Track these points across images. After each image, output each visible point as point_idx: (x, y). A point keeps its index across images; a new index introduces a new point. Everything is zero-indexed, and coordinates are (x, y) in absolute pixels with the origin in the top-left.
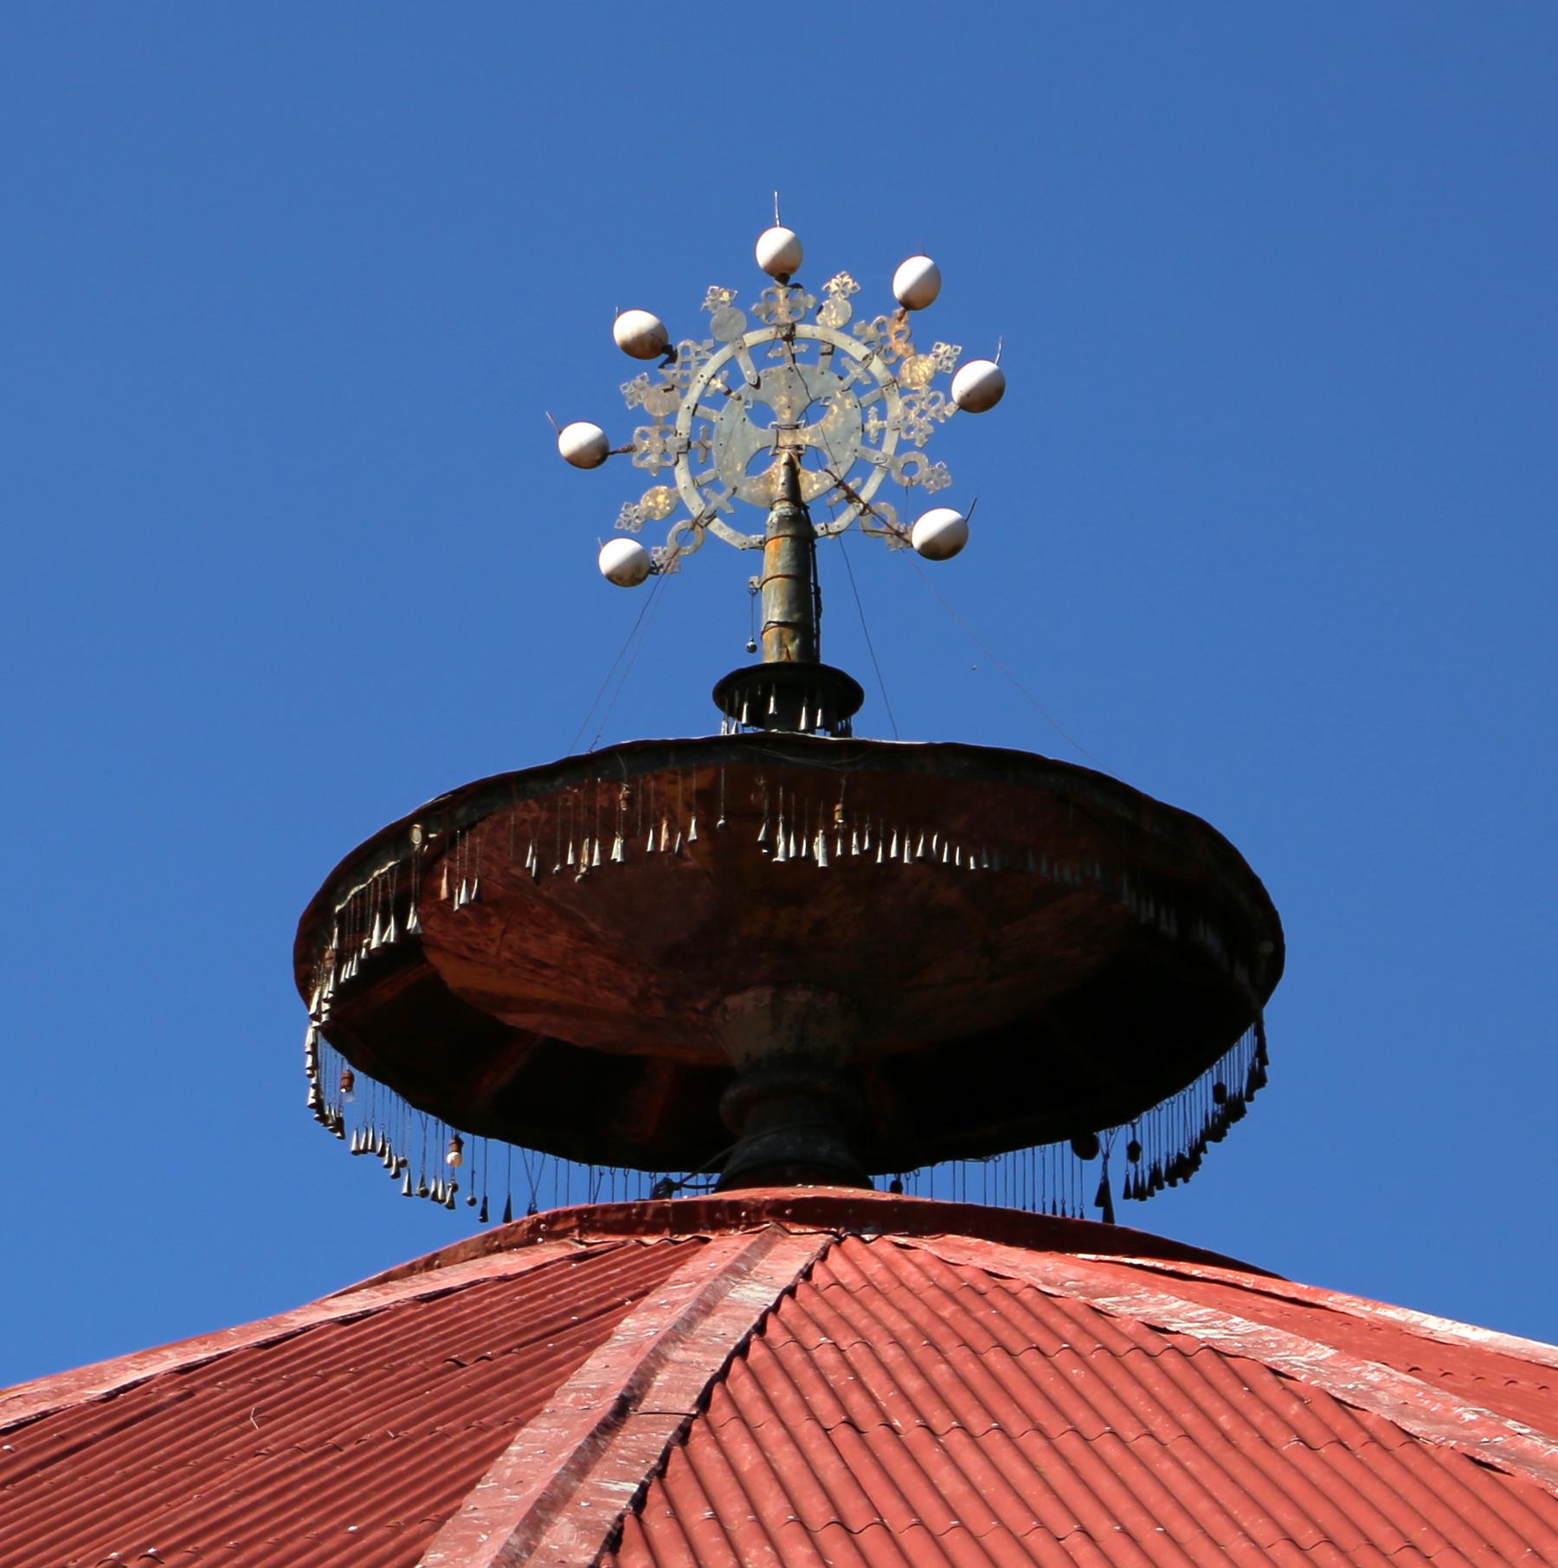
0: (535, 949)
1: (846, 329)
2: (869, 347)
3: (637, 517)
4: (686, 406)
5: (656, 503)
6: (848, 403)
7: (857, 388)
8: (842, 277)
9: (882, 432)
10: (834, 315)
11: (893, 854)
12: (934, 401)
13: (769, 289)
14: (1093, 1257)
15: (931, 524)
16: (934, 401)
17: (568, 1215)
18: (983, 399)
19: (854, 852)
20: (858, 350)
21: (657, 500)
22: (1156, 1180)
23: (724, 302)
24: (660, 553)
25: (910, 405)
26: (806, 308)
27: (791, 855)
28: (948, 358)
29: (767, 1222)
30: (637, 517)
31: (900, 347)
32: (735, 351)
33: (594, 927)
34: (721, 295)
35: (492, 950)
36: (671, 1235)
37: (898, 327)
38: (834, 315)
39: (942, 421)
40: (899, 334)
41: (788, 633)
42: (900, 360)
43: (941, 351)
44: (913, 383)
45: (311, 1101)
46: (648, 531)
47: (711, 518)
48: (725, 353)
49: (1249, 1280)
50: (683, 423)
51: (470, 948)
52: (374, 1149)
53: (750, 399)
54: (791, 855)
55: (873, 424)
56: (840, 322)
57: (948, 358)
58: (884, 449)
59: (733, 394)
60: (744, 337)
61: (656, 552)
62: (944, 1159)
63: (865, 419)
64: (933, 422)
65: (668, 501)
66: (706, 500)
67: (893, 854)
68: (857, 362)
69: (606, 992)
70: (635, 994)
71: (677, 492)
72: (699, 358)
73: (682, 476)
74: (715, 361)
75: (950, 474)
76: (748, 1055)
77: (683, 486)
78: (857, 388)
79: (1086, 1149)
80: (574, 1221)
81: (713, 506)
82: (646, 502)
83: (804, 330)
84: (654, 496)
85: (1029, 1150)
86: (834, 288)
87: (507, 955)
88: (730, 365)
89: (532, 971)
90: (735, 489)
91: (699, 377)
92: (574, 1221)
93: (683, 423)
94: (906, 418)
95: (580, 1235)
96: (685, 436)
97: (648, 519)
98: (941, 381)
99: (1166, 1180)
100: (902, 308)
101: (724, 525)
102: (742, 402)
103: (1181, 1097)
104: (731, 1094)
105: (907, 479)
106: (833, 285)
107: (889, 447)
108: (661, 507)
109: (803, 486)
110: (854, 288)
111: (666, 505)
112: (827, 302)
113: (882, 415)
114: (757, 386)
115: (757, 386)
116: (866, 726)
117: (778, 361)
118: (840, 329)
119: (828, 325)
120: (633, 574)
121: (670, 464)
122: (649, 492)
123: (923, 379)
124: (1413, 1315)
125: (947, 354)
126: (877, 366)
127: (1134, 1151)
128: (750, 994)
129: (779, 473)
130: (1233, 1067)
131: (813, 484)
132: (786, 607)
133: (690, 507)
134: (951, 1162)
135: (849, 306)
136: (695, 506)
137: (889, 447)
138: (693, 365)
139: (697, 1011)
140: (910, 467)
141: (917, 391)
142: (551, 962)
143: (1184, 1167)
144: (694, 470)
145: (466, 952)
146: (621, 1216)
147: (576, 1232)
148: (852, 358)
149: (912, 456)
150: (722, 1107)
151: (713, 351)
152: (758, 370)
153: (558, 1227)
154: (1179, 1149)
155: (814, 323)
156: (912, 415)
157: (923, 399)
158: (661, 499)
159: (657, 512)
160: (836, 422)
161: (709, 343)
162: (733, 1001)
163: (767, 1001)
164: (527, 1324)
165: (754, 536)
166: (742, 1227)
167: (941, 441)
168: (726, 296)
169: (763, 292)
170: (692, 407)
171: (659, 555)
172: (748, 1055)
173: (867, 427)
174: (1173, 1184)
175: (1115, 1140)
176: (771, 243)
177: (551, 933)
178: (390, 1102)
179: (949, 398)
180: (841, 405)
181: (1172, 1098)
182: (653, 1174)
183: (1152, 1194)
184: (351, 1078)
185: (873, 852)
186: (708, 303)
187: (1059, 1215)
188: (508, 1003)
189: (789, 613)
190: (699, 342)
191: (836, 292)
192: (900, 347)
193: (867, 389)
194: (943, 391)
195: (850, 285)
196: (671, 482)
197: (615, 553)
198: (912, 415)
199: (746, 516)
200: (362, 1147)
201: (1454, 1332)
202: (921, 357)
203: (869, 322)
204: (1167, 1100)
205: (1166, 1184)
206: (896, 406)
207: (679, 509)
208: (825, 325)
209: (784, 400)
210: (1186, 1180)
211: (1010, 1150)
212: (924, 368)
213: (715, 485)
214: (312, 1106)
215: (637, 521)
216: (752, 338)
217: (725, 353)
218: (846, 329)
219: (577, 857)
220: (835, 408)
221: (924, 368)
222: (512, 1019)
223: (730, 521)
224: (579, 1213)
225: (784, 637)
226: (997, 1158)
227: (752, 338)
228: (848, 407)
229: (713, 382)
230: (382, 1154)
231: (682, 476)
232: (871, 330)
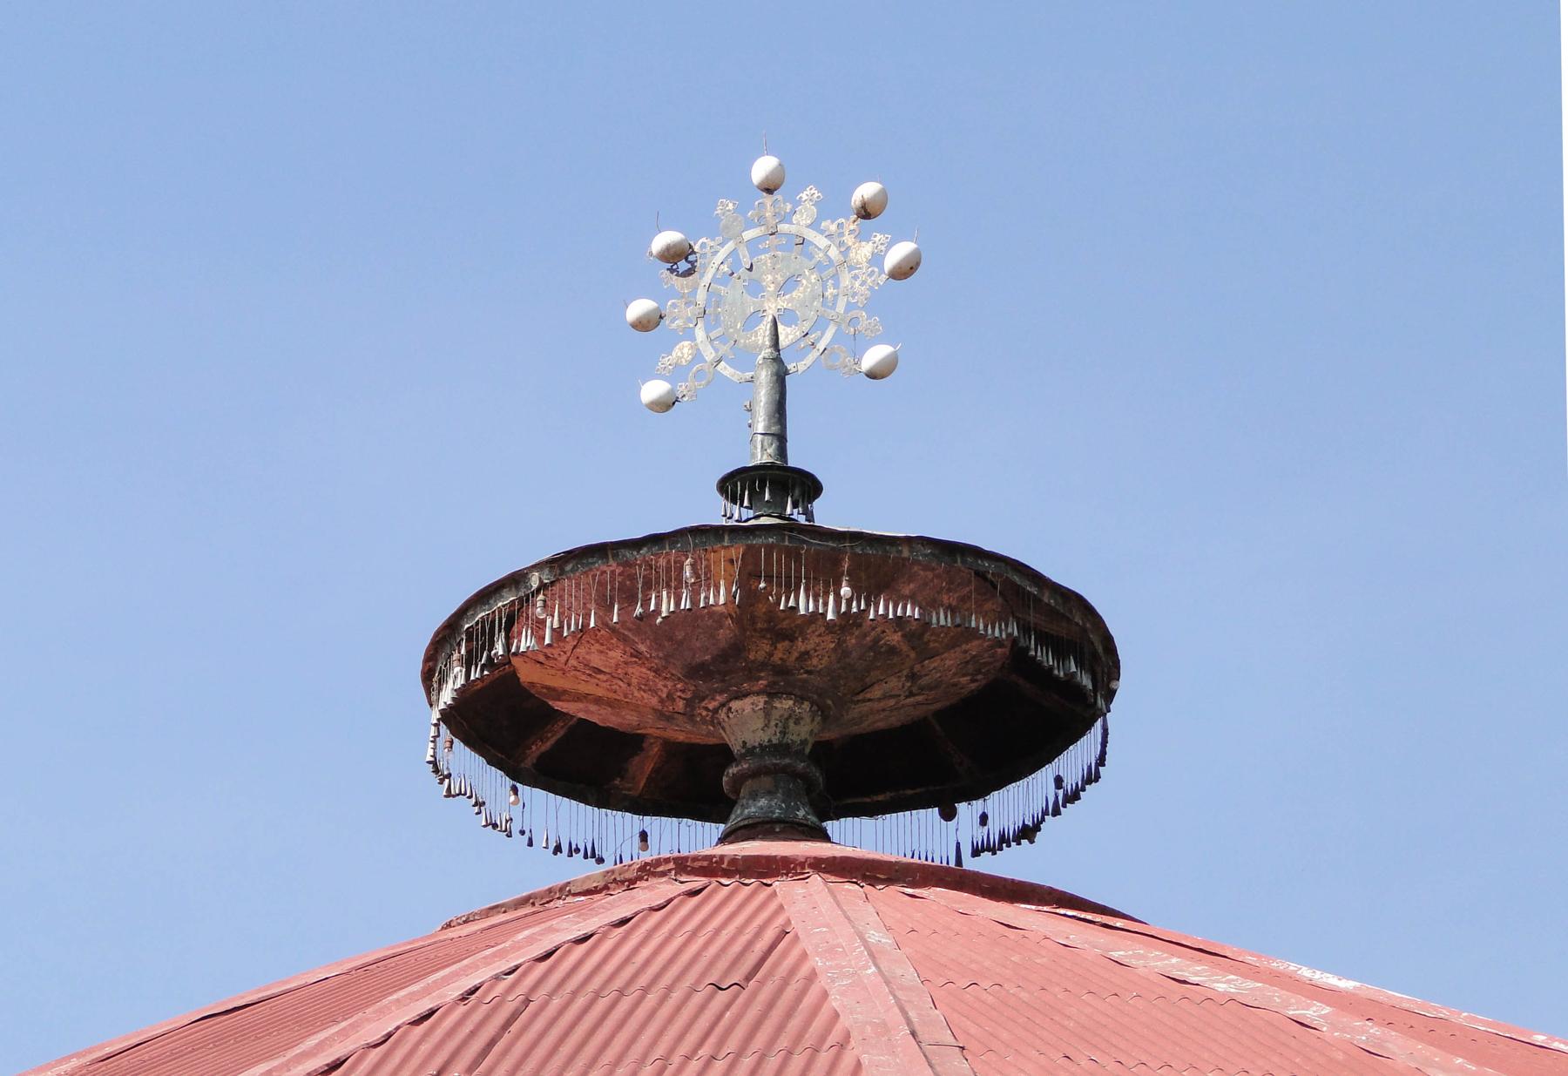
0: (596, 661)
1: (815, 225)
2: (830, 240)
3: (670, 365)
4: (703, 285)
5: (682, 353)
6: (813, 278)
7: (818, 267)
8: (811, 189)
9: (836, 297)
10: (804, 216)
11: (881, 611)
12: (871, 274)
13: (760, 201)
14: (1033, 907)
15: (874, 356)
16: (871, 274)
17: (667, 860)
18: (904, 272)
19: (855, 610)
20: (822, 242)
21: (683, 351)
22: (1004, 840)
23: (729, 211)
24: (684, 387)
25: (855, 277)
26: (785, 212)
27: (810, 611)
28: (882, 244)
29: (808, 873)
30: (670, 365)
31: (849, 240)
32: (736, 244)
33: (642, 648)
34: (727, 205)
35: (564, 658)
36: (740, 878)
37: (852, 227)
38: (804, 216)
39: (876, 288)
40: (851, 232)
41: (768, 439)
42: (849, 248)
43: (877, 239)
44: (858, 263)
45: (429, 758)
46: (677, 373)
47: (719, 361)
48: (730, 246)
49: (1119, 923)
50: (701, 296)
51: (547, 657)
52: (465, 794)
53: (747, 278)
54: (810, 611)
55: (830, 291)
56: (809, 222)
57: (882, 244)
58: (837, 310)
59: (735, 275)
60: (743, 234)
61: (681, 386)
62: (846, 816)
63: (825, 288)
64: (871, 288)
65: (690, 352)
66: (716, 350)
67: (881, 611)
68: (820, 249)
69: (642, 693)
70: (664, 696)
71: (696, 345)
72: (713, 250)
73: (700, 333)
74: (723, 253)
75: (882, 325)
76: (744, 743)
77: (700, 340)
78: (818, 267)
79: (948, 814)
80: (671, 865)
81: (720, 354)
82: (676, 353)
83: (783, 227)
84: (681, 349)
85: (908, 813)
86: (805, 197)
87: (573, 662)
88: (733, 253)
89: (590, 675)
90: (736, 341)
91: (712, 264)
92: (671, 865)
93: (701, 296)
94: (852, 287)
95: (675, 876)
96: (702, 306)
97: (677, 366)
98: (877, 259)
99: (1013, 841)
100: (856, 216)
101: (727, 366)
102: (741, 280)
103: (1026, 783)
104: (733, 770)
105: (852, 330)
106: (804, 196)
107: (841, 308)
108: (686, 356)
109: (781, 338)
110: (818, 197)
111: (689, 355)
112: (800, 207)
113: (836, 286)
114: (750, 269)
115: (750, 269)
116: (829, 513)
117: (765, 251)
118: (809, 226)
119: (800, 222)
120: (665, 405)
121: (691, 325)
122: (678, 347)
123: (865, 260)
124: (1289, 965)
125: (881, 241)
126: (834, 253)
127: (984, 819)
128: (748, 700)
129: (765, 328)
130: (1073, 761)
131: (787, 335)
132: (767, 422)
133: (705, 355)
134: (851, 818)
135: (815, 210)
136: (709, 354)
137: (841, 308)
138: (709, 255)
139: (706, 709)
140: (853, 321)
141: (860, 268)
142: (604, 670)
143: (1027, 833)
144: (708, 331)
145: (542, 659)
146: (705, 864)
147: (673, 872)
148: (816, 247)
149: (854, 313)
150: (725, 779)
151: (722, 245)
152: (751, 258)
153: (660, 869)
154: (1024, 821)
155: (791, 223)
156: (857, 284)
157: (864, 273)
158: (686, 350)
159: (683, 360)
160: (805, 291)
161: (719, 239)
162: (735, 705)
163: (761, 705)
164: (548, 924)
165: (747, 374)
166: (790, 875)
167: (874, 303)
168: (731, 206)
169: (757, 203)
170: (707, 285)
171: (681, 389)
172: (744, 743)
173: (826, 294)
174: (1019, 844)
175: (967, 811)
176: (763, 167)
177: (610, 650)
178: (958, 845)
179: (882, 270)
180: (808, 280)
181: (1018, 783)
182: (641, 817)
183: (1001, 849)
184: (452, 742)
185: (867, 611)
186: (719, 212)
187: (945, 864)
188: (560, 694)
189: (768, 427)
190: (713, 240)
191: (806, 200)
192: (849, 240)
193: (828, 267)
194: (878, 267)
195: (816, 195)
196: (693, 338)
197: (653, 390)
198: (857, 284)
199: (741, 358)
200: (457, 792)
201: (1325, 980)
202: (864, 243)
203: (833, 222)
204: (1014, 784)
205: (1013, 844)
206: (846, 280)
207: (697, 356)
208: (798, 224)
209: (770, 277)
210: (1032, 842)
211: (894, 812)
212: (864, 251)
213: (722, 338)
214: (429, 762)
215: (670, 367)
216: (749, 235)
217: (730, 246)
218: (815, 225)
219: (659, 604)
220: (804, 282)
221: (864, 251)
222: (558, 705)
223: (731, 364)
224: (676, 860)
225: (766, 444)
226: (884, 817)
227: (749, 235)
228: (813, 281)
229: (722, 266)
230: (470, 797)
231: (700, 333)
232: (833, 227)
